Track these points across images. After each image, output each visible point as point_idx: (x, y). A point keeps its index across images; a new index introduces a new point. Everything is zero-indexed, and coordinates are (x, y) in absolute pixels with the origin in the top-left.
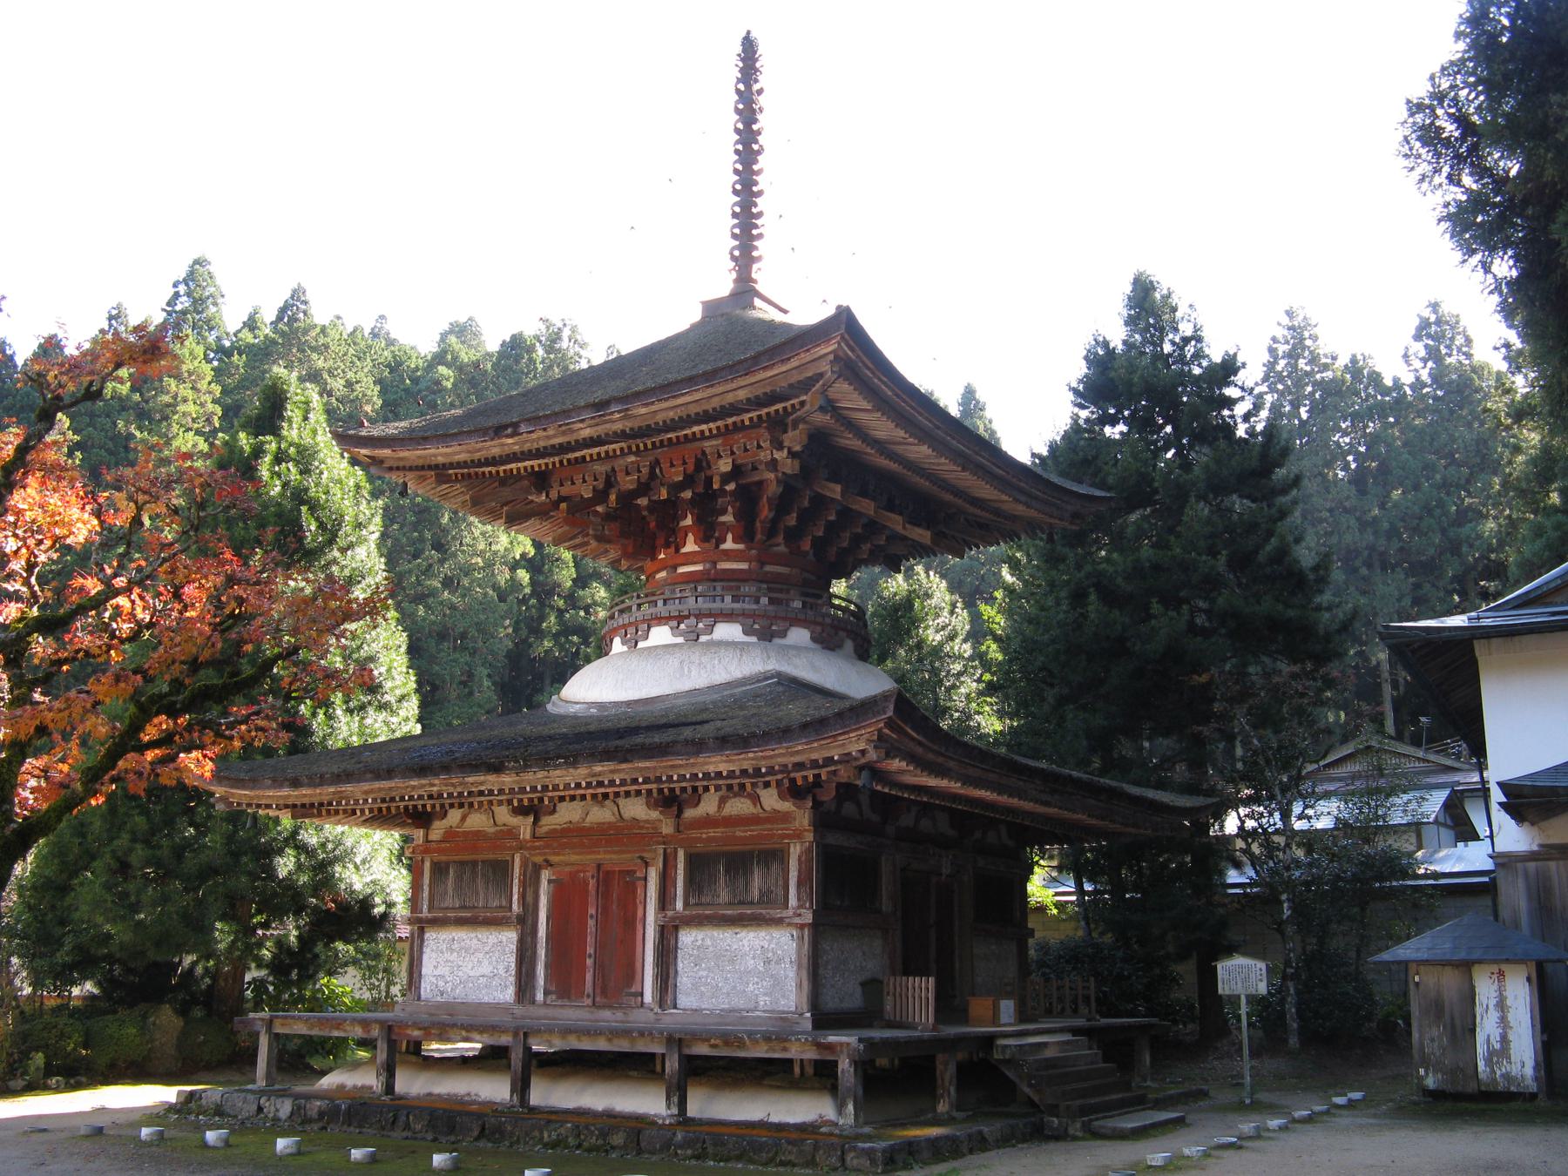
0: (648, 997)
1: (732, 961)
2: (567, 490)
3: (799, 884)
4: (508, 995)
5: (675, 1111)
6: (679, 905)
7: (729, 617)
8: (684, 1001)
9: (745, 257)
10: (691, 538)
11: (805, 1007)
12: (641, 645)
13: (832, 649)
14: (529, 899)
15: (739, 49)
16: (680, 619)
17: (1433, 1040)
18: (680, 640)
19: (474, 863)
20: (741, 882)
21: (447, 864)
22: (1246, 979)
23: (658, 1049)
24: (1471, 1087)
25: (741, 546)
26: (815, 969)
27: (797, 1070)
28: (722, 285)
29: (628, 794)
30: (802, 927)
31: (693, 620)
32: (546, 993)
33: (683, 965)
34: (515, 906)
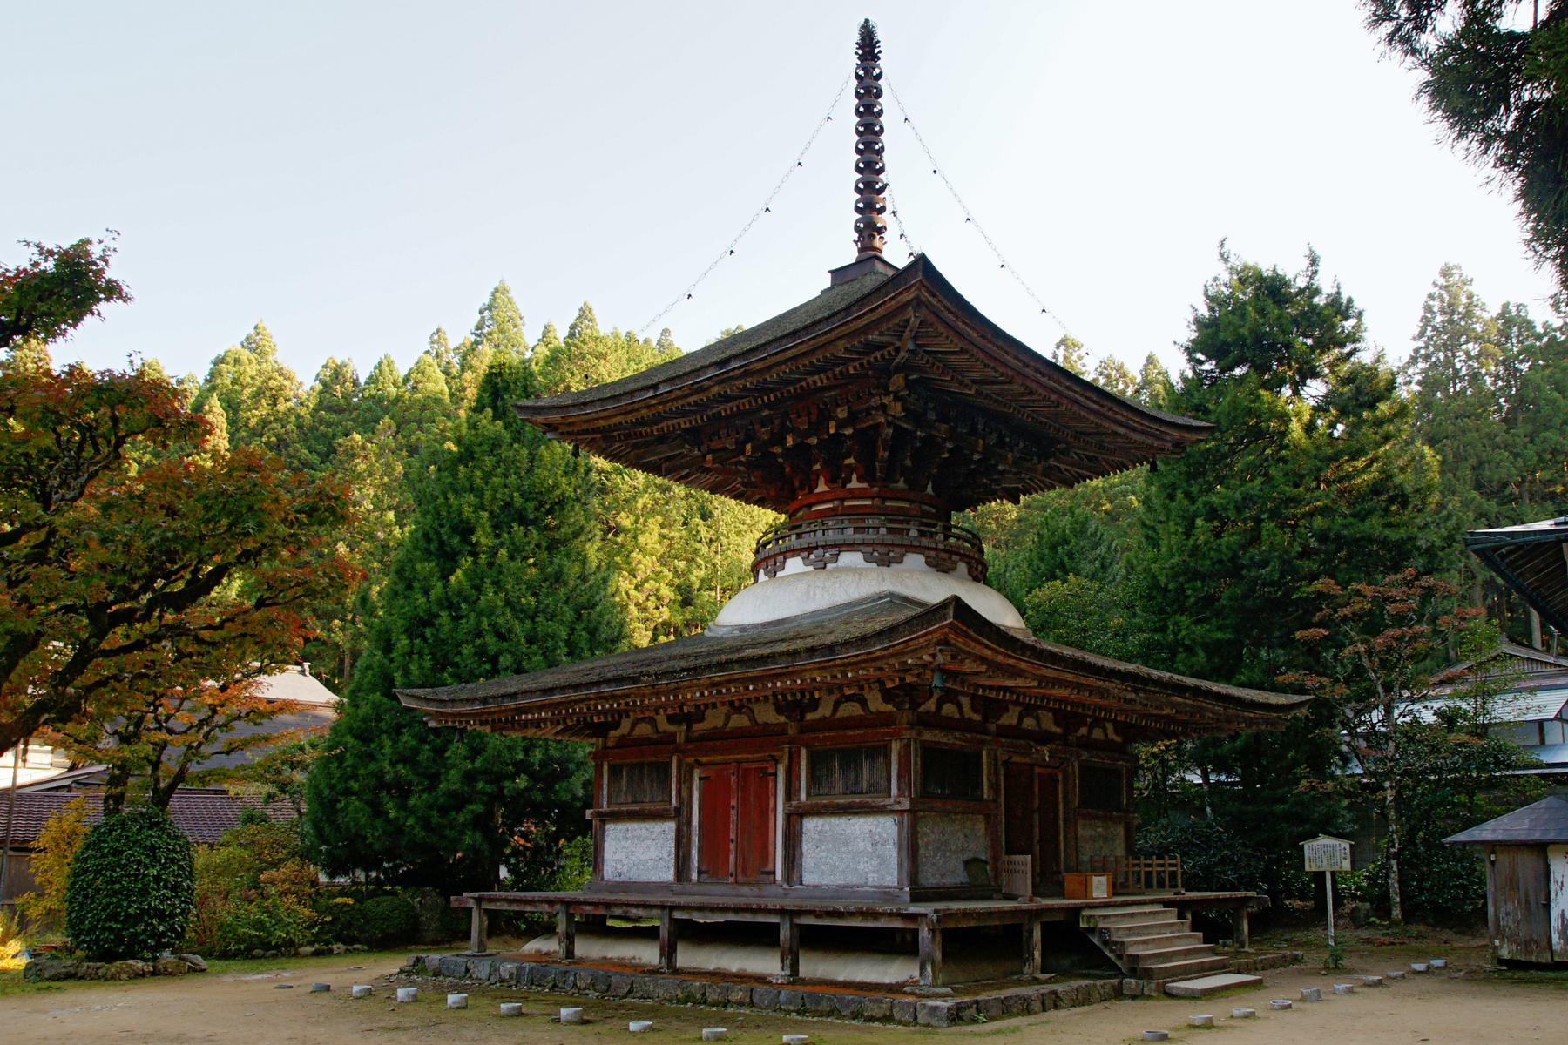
0: (779, 876)
1: (846, 844)
2: (715, 445)
3: (900, 776)
4: (669, 875)
5: (788, 972)
6: (803, 796)
7: (851, 546)
8: (809, 878)
9: (869, 231)
10: (822, 479)
11: (906, 882)
12: (779, 574)
13: (945, 571)
14: (684, 794)
15: (856, 38)
16: (810, 549)
17: (1507, 914)
18: (811, 568)
19: (641, 765)
20: (852, 776)
21: (621, 766)
22: (1332, 857)
23: (774, 919)
24: (1545, 958)
25: (865, 485)
26: (911, 850)
27: (898, 939)
28: (850, 255)
29: (757, 699)
30: (902, 812)
31: (820, 551)
32: (699, 873)
33: (807, 846)
34: (674, 801)
